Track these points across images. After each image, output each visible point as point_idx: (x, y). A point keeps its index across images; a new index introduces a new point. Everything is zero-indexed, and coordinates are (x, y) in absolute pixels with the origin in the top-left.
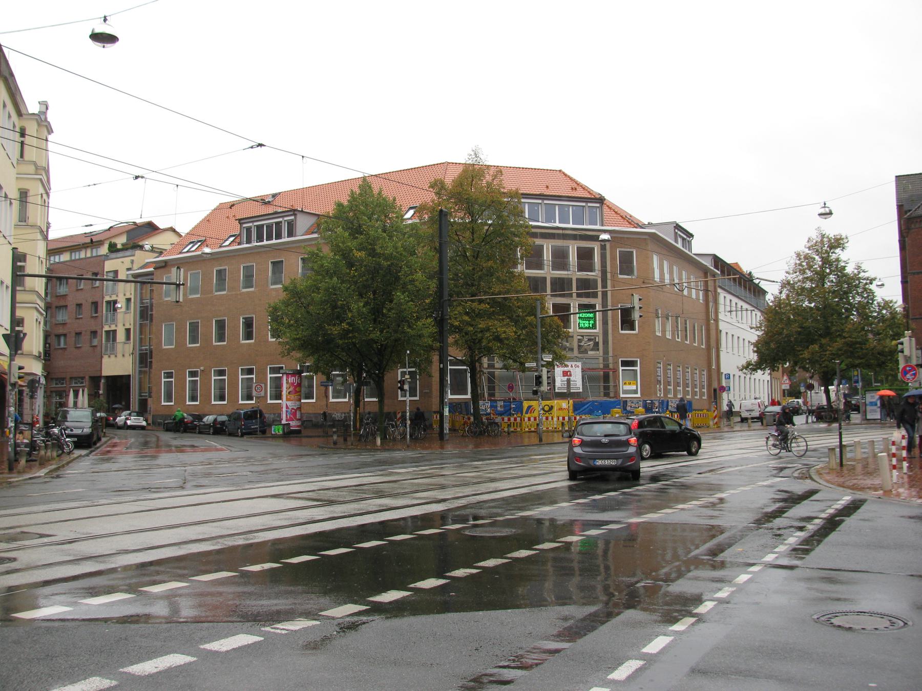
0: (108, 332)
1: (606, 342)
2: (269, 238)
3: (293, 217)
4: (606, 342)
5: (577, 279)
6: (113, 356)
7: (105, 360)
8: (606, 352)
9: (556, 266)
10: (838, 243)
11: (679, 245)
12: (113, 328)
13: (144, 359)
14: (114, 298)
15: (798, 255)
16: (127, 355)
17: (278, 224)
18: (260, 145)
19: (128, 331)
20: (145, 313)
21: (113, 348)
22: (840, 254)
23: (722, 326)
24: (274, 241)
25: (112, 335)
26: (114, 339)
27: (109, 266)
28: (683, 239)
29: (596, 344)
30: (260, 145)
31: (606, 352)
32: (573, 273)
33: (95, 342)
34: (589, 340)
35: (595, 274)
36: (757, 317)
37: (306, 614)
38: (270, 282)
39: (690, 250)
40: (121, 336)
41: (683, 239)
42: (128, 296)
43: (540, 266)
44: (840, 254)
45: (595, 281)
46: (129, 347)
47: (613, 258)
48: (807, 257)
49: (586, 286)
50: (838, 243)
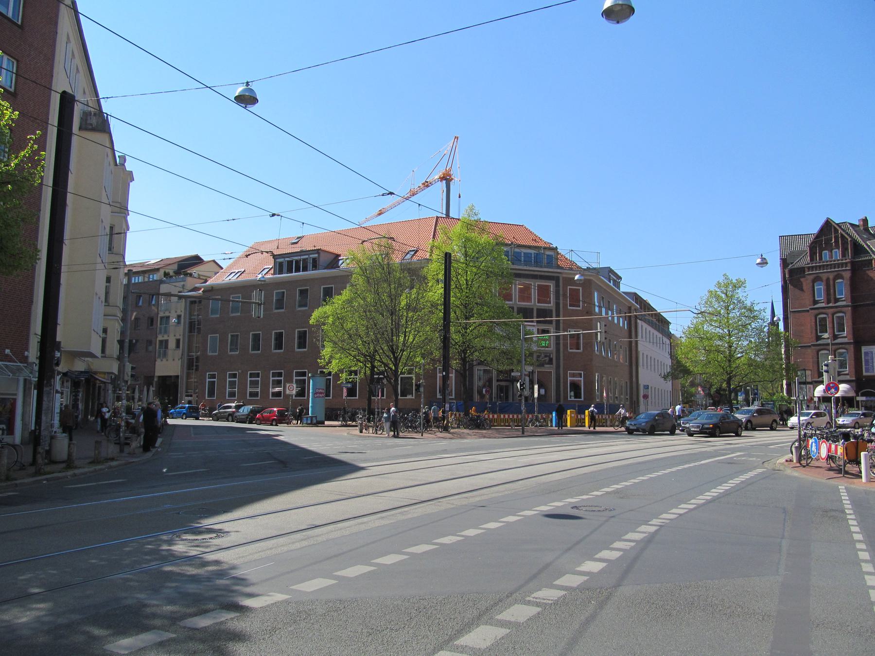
0: (161, 342)
1: (558, 358)
2: (298, 270)
3: (316, 255)
4: (558, 358)
5: (538, 309)
6: (164, 360)
7: (159, 363)
8: (558, 367)
9: (522, 299)
10: (739, 285)
11: (611, 284)
12: (166, 338)
13: (191, 364)
14: (167, 314)
15: (710, 292)
16: (176, 359)
17: (304, 260)
18: (391, 193)
19: (178, 341)
20: (193, 327)
21: (165, 355)
22: (740, 293)
23: (640, 349)
24: (294, 274)
25: (165, 344)
26: (166, 347)
27: (164, 288)
28: (614, 281)
29: (551, 360)
30: (391, 193)
31: (558, 367)
32: (534, 303)
33: (150, 348)
34: (546, 356)
35: (552, 305)
36: (65, 346)
37: (535, 576)
38: (297, 304)
39: (619, 288)
40: (172, 344)
41: (614, 281)
42: (179, 313)
43: (529, 299)
44: (740, 293)
45: (551, 311)
46: (179, 352)
47: (565, 295)
48: (325, 301)
49: (543, 313)
50: (739, 285)
